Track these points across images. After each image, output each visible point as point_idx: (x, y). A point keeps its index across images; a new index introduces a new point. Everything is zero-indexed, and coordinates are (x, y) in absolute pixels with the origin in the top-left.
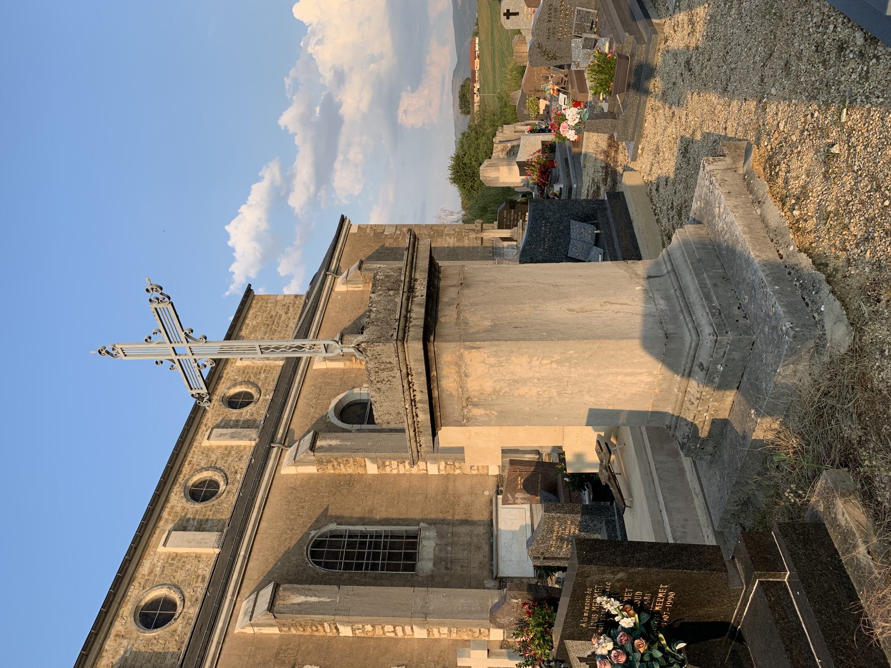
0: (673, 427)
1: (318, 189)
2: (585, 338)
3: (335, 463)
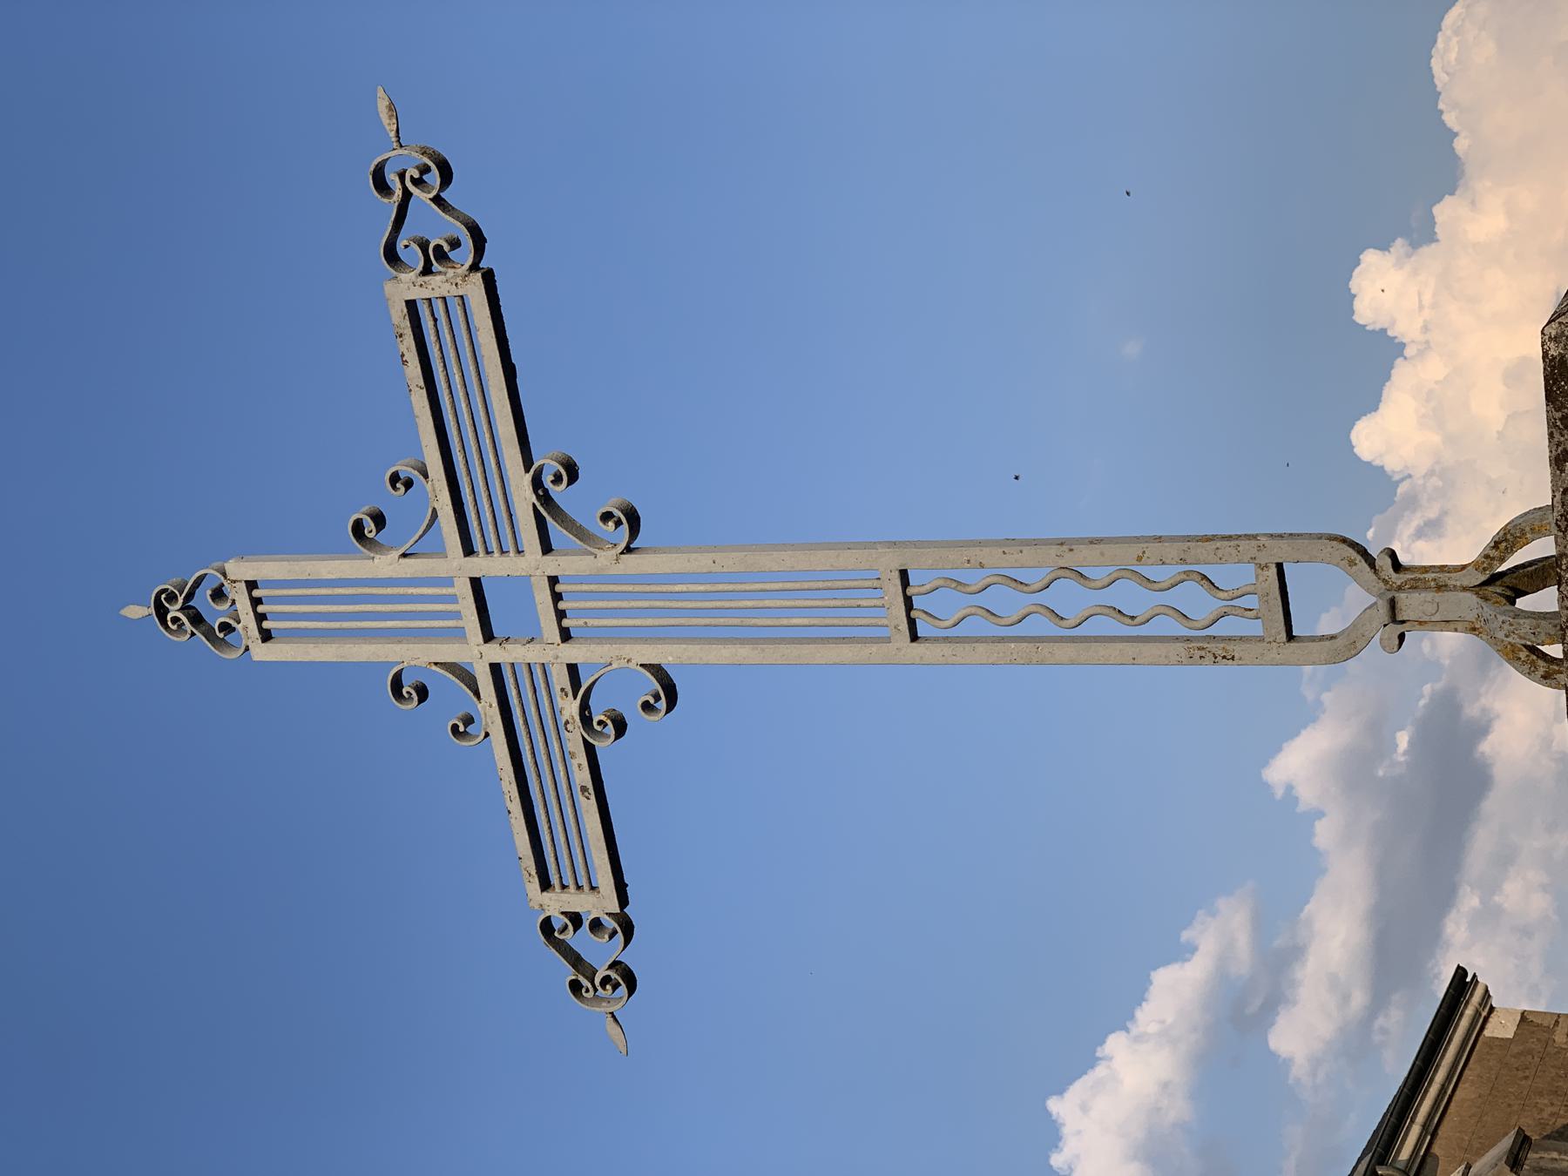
1: (1378, 1002)
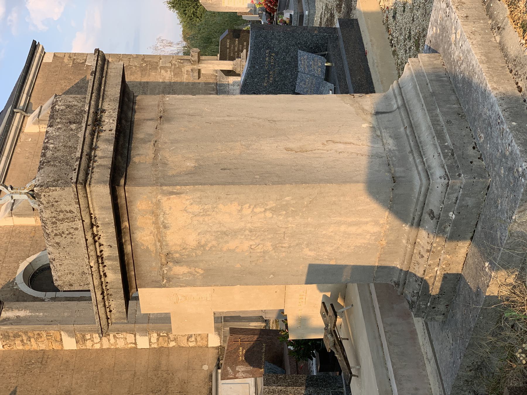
0: (401, 283)
1: (8, 12)
2: (303, 181)
3: (25, 338)
